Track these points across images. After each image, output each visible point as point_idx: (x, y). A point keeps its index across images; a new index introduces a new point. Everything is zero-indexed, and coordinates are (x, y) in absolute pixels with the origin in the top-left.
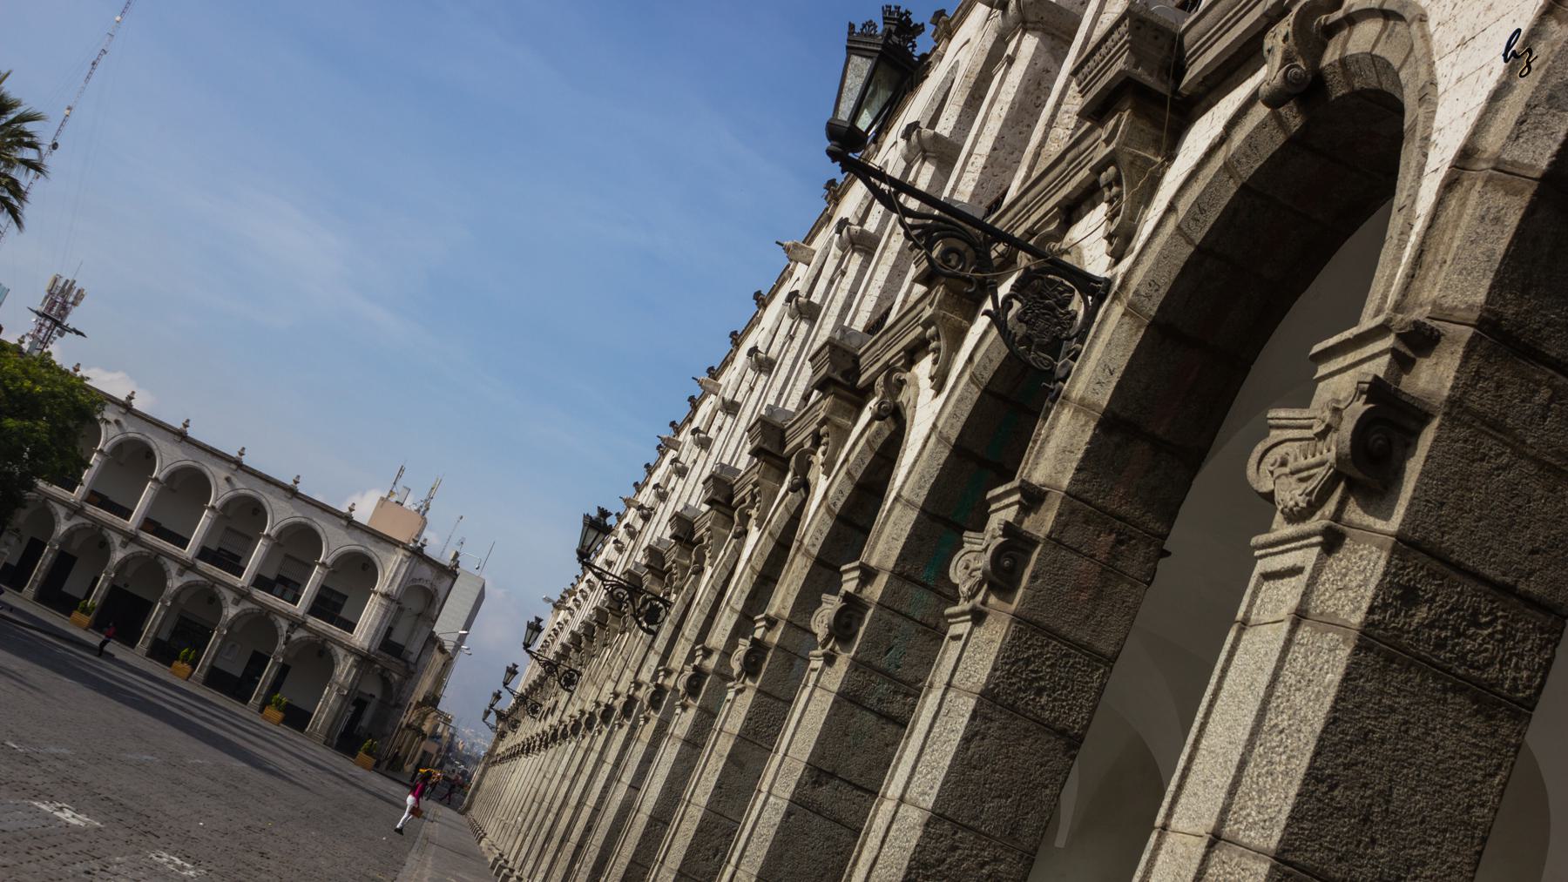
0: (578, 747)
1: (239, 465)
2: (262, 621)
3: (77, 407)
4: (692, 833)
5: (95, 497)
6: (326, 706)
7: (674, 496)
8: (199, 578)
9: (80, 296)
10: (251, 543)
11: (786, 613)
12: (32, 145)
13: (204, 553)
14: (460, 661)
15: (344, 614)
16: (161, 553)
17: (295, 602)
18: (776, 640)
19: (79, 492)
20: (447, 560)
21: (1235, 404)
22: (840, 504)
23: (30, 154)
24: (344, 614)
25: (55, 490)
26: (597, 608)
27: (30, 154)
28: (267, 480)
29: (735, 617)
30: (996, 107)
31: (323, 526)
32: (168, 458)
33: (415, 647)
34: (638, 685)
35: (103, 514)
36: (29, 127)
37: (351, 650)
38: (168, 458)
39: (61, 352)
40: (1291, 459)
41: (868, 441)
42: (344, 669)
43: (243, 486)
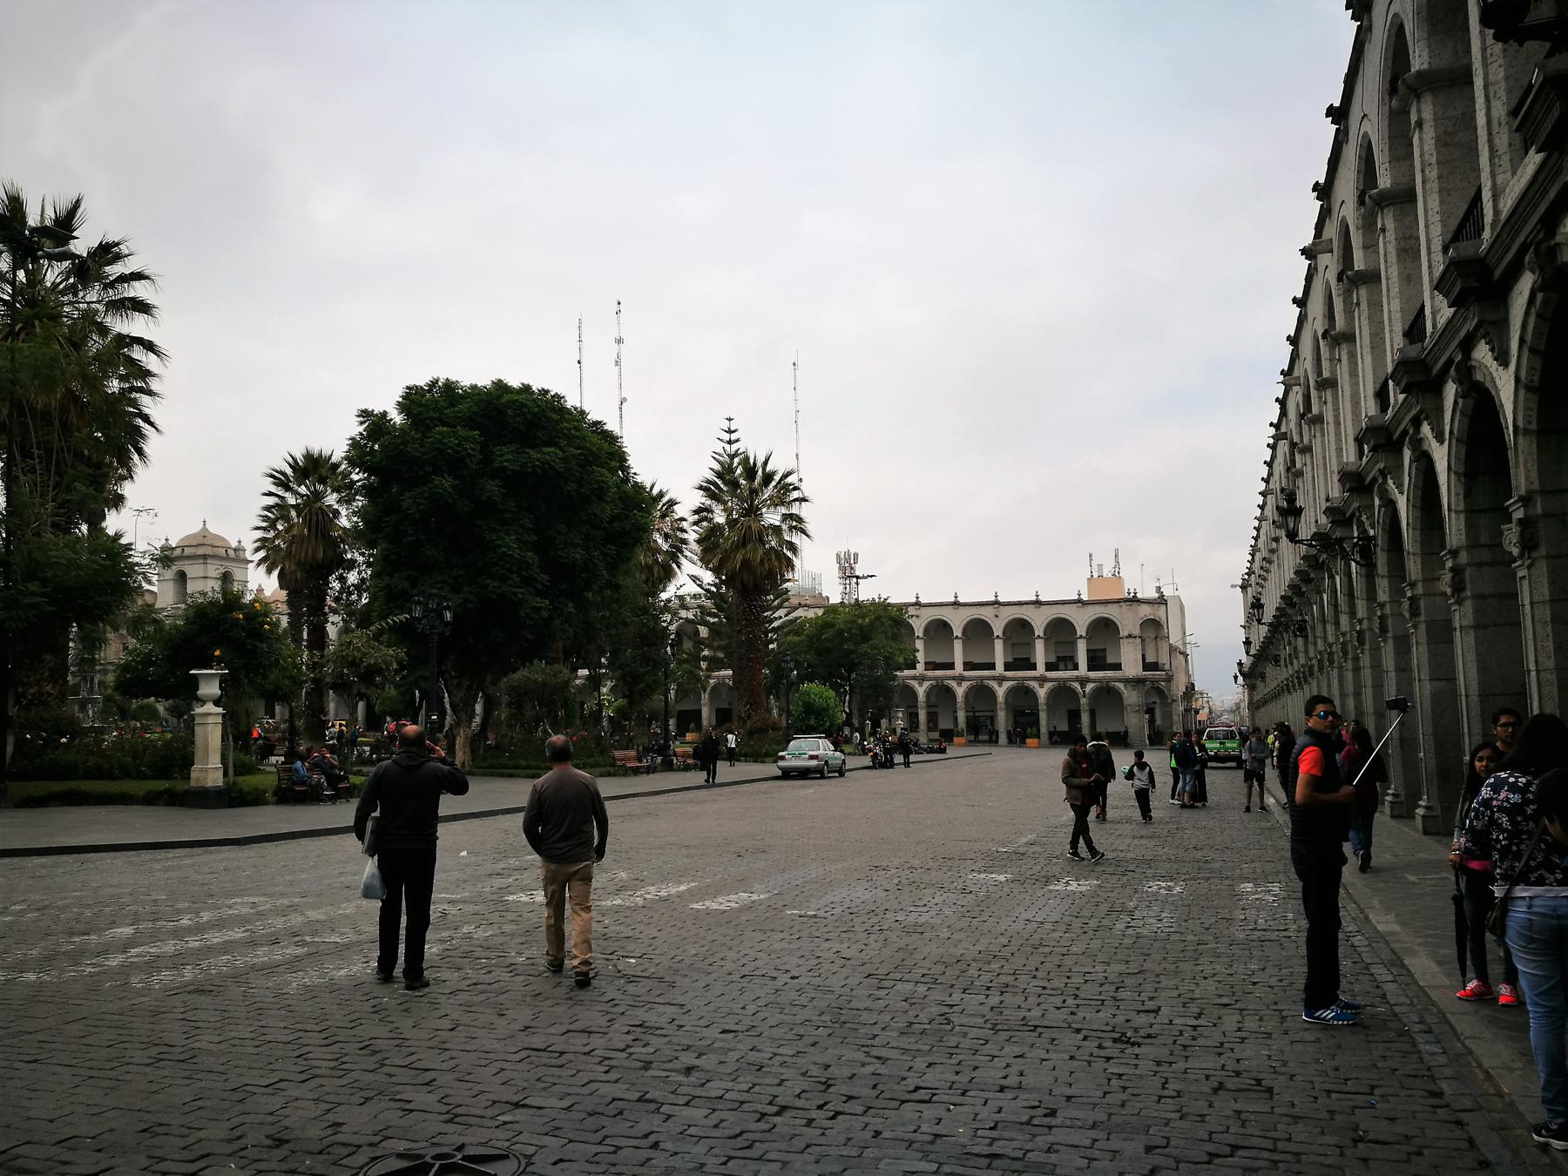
1: (996, 603)
2: (1062, 693)
3: (886, 622)
4: (1556, 694)
5: (930, 666)
6: (1002, 720)
8: (1010, 683)
9: (856, 556)
10: (1073, 644)
11: (1536, 486)
12: (796, 489)
15: (1110, 660)
16: (982, 678)
17: (1076, 667)
18: (1539, 511)
19: (920, 667)
20: (1150, 593)
22: (1536, 379)
23: (795, 494)
24: (1110, 660)
25: (907, 673)
27: (795, 494)
28: (1020, 604)
29: (1462, 517)
32: (957, 622)
33: (1164, 659)
34: (1330, 646)
35: (939, 673)
36: (789, 480)
37: (1126, 681)
38: (957, 622)
39: (867, 592)
41: (1538, 315)
42: (1131, 697)
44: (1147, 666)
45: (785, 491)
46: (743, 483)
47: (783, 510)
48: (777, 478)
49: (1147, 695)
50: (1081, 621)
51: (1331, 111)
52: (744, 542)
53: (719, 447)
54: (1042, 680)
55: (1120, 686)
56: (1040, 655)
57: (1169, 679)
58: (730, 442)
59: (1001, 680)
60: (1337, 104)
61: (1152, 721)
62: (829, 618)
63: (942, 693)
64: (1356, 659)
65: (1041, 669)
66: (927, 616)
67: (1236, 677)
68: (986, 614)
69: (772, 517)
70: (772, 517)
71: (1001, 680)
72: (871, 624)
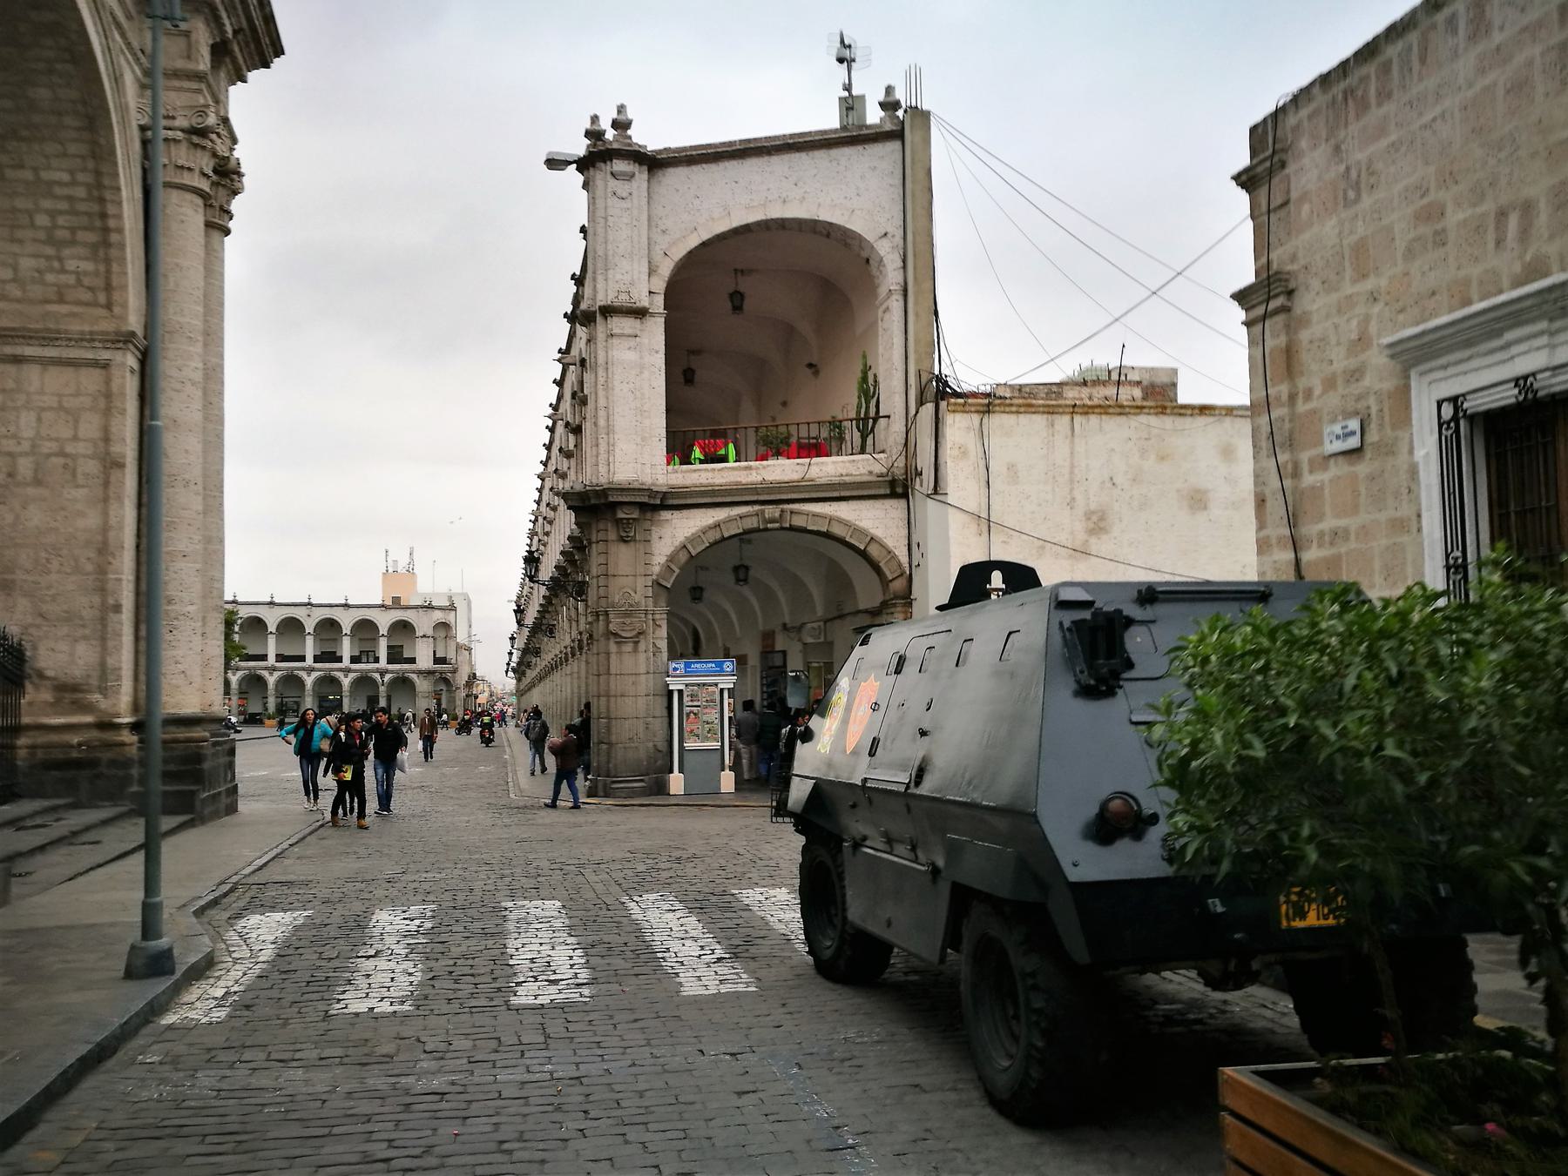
2: (364, 681)
7: (411, 1116)
13: (317, 659)
21: (1128, 877)
30: (710, 475)
32: (272, 619)
33: (451, 655)
37: (420, 672)
38: (272, 619)
40: (1300, 255)
42: (422, 685)
44: (438, 660)
49: (436, 683)
50: (384, 621)
54: (347, 671)
56: (346, 649)
57: (455, 671)
59: (310, 670)
65: (346, 662)
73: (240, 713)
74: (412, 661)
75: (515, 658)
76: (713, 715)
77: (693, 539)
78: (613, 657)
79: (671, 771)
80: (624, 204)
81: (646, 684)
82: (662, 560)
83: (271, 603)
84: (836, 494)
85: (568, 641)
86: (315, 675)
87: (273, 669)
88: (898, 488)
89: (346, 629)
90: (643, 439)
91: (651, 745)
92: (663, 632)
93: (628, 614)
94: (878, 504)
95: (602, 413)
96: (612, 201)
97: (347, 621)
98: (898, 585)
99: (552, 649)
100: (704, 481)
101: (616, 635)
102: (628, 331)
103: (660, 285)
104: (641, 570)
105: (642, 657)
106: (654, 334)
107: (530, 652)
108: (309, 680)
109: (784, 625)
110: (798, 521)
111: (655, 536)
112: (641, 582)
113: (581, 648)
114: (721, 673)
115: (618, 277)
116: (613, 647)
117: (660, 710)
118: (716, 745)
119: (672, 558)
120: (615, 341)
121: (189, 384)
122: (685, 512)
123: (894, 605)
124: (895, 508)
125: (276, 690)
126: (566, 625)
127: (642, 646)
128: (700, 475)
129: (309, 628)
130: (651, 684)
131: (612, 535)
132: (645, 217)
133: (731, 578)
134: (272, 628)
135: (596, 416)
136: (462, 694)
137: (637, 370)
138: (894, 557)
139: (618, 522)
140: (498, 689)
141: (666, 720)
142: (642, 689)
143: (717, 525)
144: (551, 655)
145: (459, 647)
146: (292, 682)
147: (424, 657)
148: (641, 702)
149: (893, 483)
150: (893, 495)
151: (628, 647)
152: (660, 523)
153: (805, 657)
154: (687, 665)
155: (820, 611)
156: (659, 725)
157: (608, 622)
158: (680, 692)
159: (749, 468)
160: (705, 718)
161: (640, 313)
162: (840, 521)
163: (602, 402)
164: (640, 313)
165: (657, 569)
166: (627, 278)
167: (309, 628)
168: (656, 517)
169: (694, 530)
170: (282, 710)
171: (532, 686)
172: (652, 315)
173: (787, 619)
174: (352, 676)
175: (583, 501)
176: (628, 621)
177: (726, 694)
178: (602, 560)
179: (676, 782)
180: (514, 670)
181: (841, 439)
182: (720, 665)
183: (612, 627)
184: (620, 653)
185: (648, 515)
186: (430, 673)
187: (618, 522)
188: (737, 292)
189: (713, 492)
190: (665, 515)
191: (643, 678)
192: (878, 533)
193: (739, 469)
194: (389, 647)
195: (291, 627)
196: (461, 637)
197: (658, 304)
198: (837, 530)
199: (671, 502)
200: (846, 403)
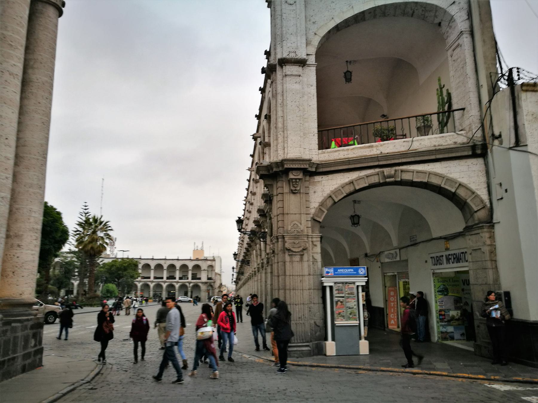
0: (266, 273)
14: (223, 275)
15: (198, 277)
17: (188, 279)
23: (110, 228)
26: (247, 244)
27: (110, 228)
30: (346, 153)
31: (186, 263)
32: (153, 264)
33: (213, 277)
34: (263, 260)
37: (202, 283)
38: (153, 264)
42: (203, 287)
43: (169, 263)
44: (209, 279)
45: (106, 227)
46: (92, 225)
47: (104, 232)
48: (104, 223)
49: (208, 287)
50: (190, 265)
51: (256, 116)
52: (90, 242)
53: (82, 211)
54: (177, 282)
55: (200, 284)
56: (178, 275)
57: (214, 282)
58: (85, 209)
59: (165, 282)
60: (258, 114)
61: (209, 294)
62: (113, 263)
63: (146, 286)
64: (266, 269)
65: (177, 279)
66: (143, 262)
67: (233, 268)
68: (162, 262)
69: (100, 234)
70: (100, 234)
71: (165, 282)
72: (128, 266)
73: (142, 297)
74: (200, 279)
75: (235, 276)
76: (352, 303)
77: (336, 191)
78: (288, 264)
79: (326, 339)
80: (291, 8)
81: (309, 282)
82: (316, 205)
83: (153, 259)
84: (433, 157)
85: (255, 265)
86: (167, 284)
87: (152, 282)
88: (479, 151)
89: (178, 268)
90: (304, 134)
91: (312, 322)
92: (318, 249)
93: (297, 237)
94: (463, 162)
95: (280, 120)
96: (285, 6)
97: (178, 265)
98: (482, 214)
99: (248, 271)
100: (343, 157)
101: (289, 250)
102: (295, 73)
103: (313, 50)
104: (304, 210)
105: (305, 264)
106: (310, 75)
107: (240, 273)
108: (164, 286)
109: (366, 255)
110: (407, 177)
111: (311, 192)
112: (304, 218)
113: (262, 267)
114: (357, 275)
115: (289, 45)
116: (287, 258)
117: (317, 299)
118: (356, 323)
119: (322, 204)
120: (288, 79)
121: (7, 74)
122: (330, 176)
123: (482, 227)
124: (477, 164)
125: (166, 289)
126: (255, 259)
127: (305, 258)
128: (336, 153)
129: (165, 267)
130: (312, 282)
131: (286, 190)
132: (303, 15)
133: (349, 222)
134: (153, 267)
135: (276, 123)
136: (217, 291)
137: (301, 91)
138: (477, 196)
139: (290, 181)
140: (230, 289)
141: (321, 306)
142: (306, 285)
143: (351, 182)
144: (248, 274)
145: (216, 274)
146: (159, 286)
147: (204, 277)
148: (306, 293)
149: (474, 147)
150: (474, 155)
151: (297, 258)
152: (314, 183)
153: (382, 270)
154: (335, 270)
155: (395, 244)
156: (317, 309)
157: (284, 242)
158: (331, 288)
159: (372, 147)
160: (349, 305)
161: (302, 63)
162: (436, 175)
163: (280, 114)
164: (302, 63)
165: (313, 211)
166: (294, 45)
167: (165, 267)
168: (312, 180)
169: (336, 186)
170: (155, 296)
171: (241, 287)
172: (309, 65)
173: (368, 251)
174: (179, 284)
175: (269, 171)
176: (297, 241)
177: (360, 289)
178: (280, 204)
179: (331, 347)
180: (235, 282)
181: (430, 127)
182: (356, 270)
183: (287, 245)
184: (292, 262)
185: (308, 178)
186: (206, 283)
187: (290, 181)
188: (348, 71)
189: (349, 161)
190: (318, 178)
191: (306, 278)
192: (464, 181)
193: (361, 148)
194: (192, 274)
195: (159, 267)
196: (217, 270)
197: (312, 60)
198: (435, 181)
199: (321, 170)
200: (431, 105)
